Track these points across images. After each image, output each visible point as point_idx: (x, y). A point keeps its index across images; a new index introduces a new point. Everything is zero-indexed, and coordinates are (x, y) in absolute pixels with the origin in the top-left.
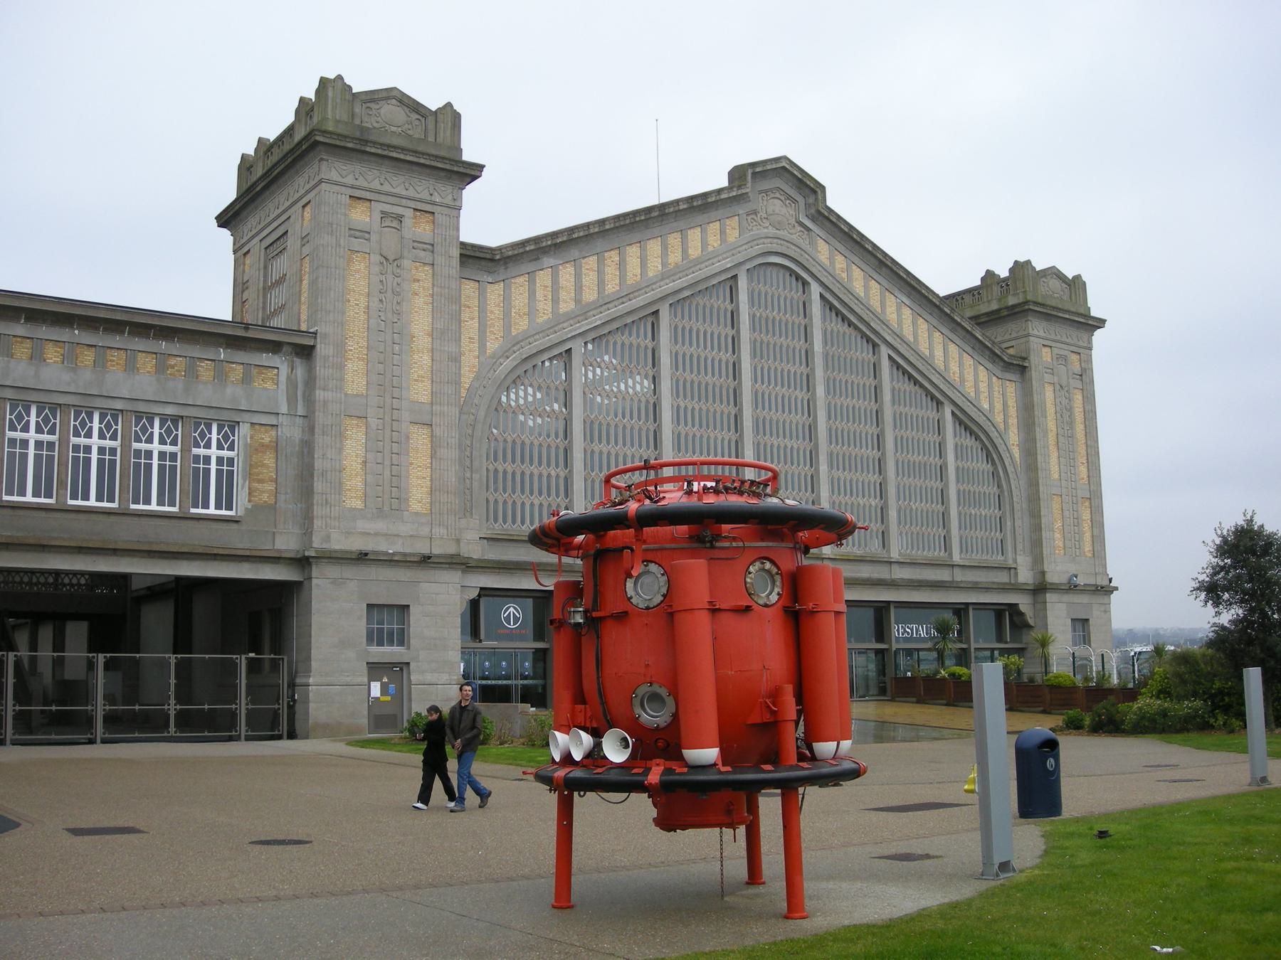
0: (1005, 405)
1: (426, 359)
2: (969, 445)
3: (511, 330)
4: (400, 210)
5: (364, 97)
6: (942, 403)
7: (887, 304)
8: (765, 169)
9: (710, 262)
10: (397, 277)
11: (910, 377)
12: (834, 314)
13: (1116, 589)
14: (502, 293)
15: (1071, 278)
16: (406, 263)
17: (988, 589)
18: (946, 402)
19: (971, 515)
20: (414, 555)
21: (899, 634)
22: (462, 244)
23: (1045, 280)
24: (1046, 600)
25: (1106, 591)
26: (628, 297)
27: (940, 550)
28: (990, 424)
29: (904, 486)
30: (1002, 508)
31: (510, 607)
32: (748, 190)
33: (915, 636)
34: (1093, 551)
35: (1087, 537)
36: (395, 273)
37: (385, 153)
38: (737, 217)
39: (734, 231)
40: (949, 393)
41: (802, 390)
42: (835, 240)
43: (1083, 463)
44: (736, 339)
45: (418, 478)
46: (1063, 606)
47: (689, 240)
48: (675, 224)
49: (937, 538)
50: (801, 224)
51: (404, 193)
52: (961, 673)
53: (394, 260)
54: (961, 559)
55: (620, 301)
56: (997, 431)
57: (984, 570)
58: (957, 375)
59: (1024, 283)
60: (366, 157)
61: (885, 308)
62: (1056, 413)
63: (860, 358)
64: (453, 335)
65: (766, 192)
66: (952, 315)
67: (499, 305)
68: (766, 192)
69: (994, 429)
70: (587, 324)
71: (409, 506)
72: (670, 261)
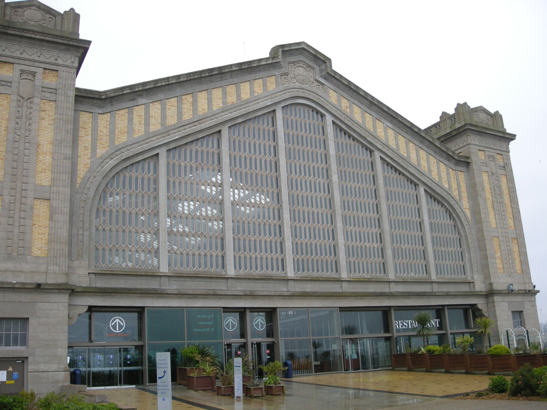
0: (459, 185)
1: (48, 159)
2: (438, 209)
3: (114, 142)
4: (33, 69)
5: (13, 5)
6: (418, 185)
7: (377, 127)
8: (291, 48)
9: (256, 102)
10: (30, 109)
11: (396, 170)
12: (343, 134)
13: (538, 291)
14: (109, 120)
15: (493, 113)
16: (36, 100)
17: (455, 295)
18: (420, 184)
19: (442, 251)
20: (30, 284)
21: (399, 327)
22: (78, 90)
23: (477, 114)
24: (494, 300)
25: (533, 293)
26: (198, 122)
27: (423, 273)
28: (450, 196)
29: (396, 235)
30: (462, 246)
31: (117, 318)
32: (279, 60)
33: (410, 327)
34: (522, 270)
35: (517, 261)
36: (29, 106)
37: (22, 34)
38: (274, 77)
39: (272, 85)
40: (422, 179)
41: (323, 177)
42: (340, 90)
43: (510, 218)
44: (276, 148)
45: (39, 234)
46: (506, 304)
47: (241, 89)
48: (231, 80)
49: (420, 266)
50: (318, 81)
51: (37, 59)
52: (434, 350)
53: (29, 99)
54: (437, 278)
55: (193, 124)
56: (455, 200)
57: (453, 284)
58: (426, 168)
59: (464, 115)
60: (9, 38)
61: (376, 130)
62: (491, 189)
63: (362, 159)
64: (68, 143)
65: (294, 63)
66: (419, 132)
67: (106, 127)
68: (294, 63)
69: (452, 199)
70: (169, 138)
71: (31, 252)
72: (228, 101)
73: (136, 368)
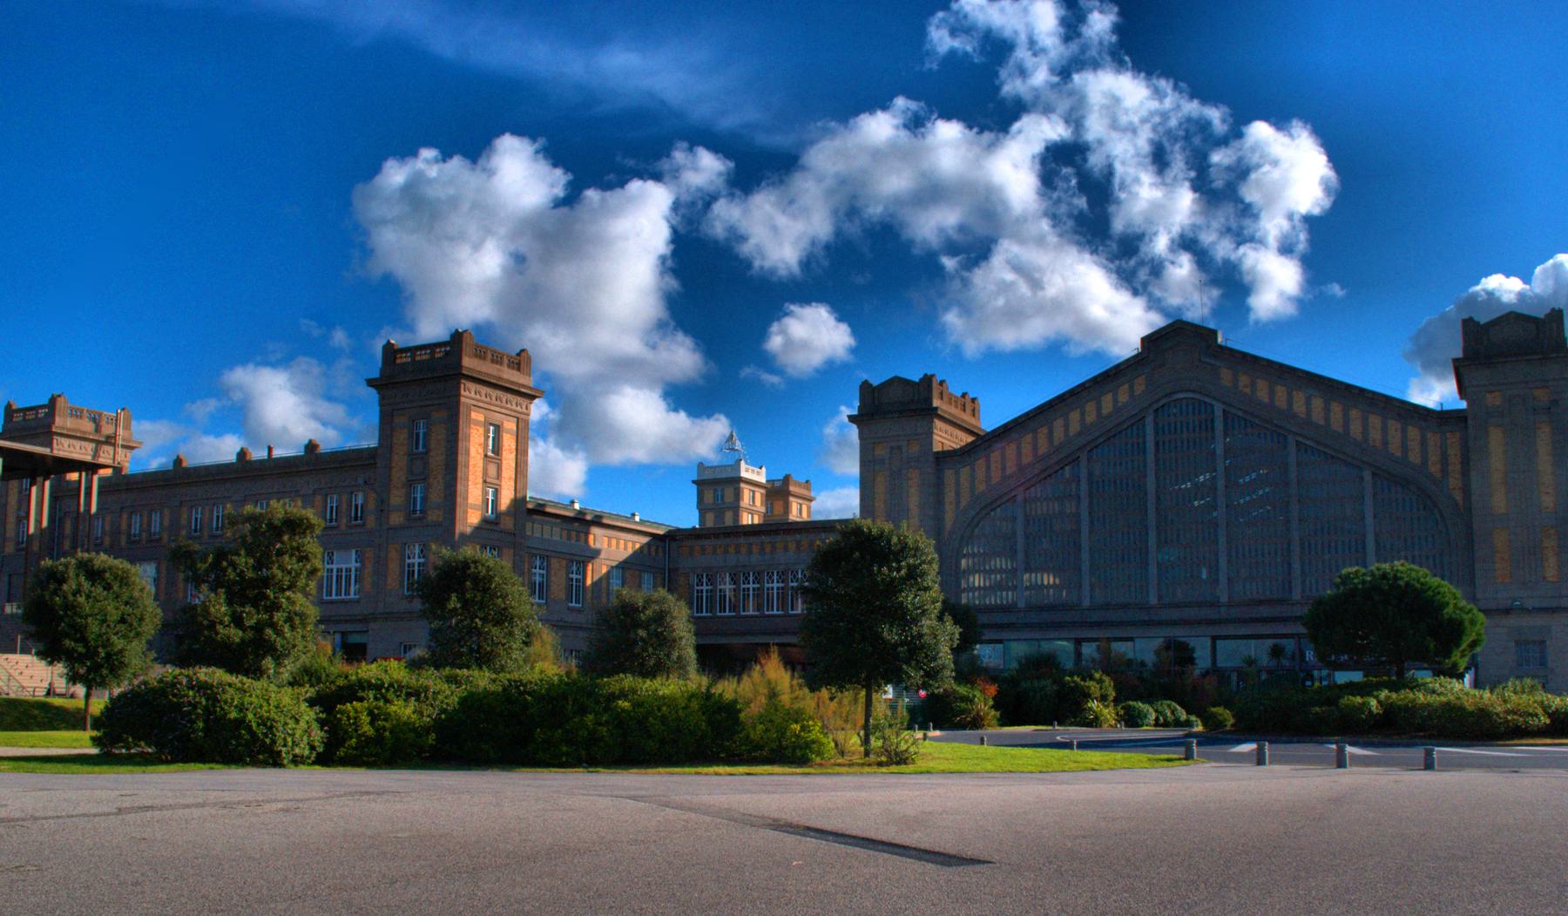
73: (471, 500)
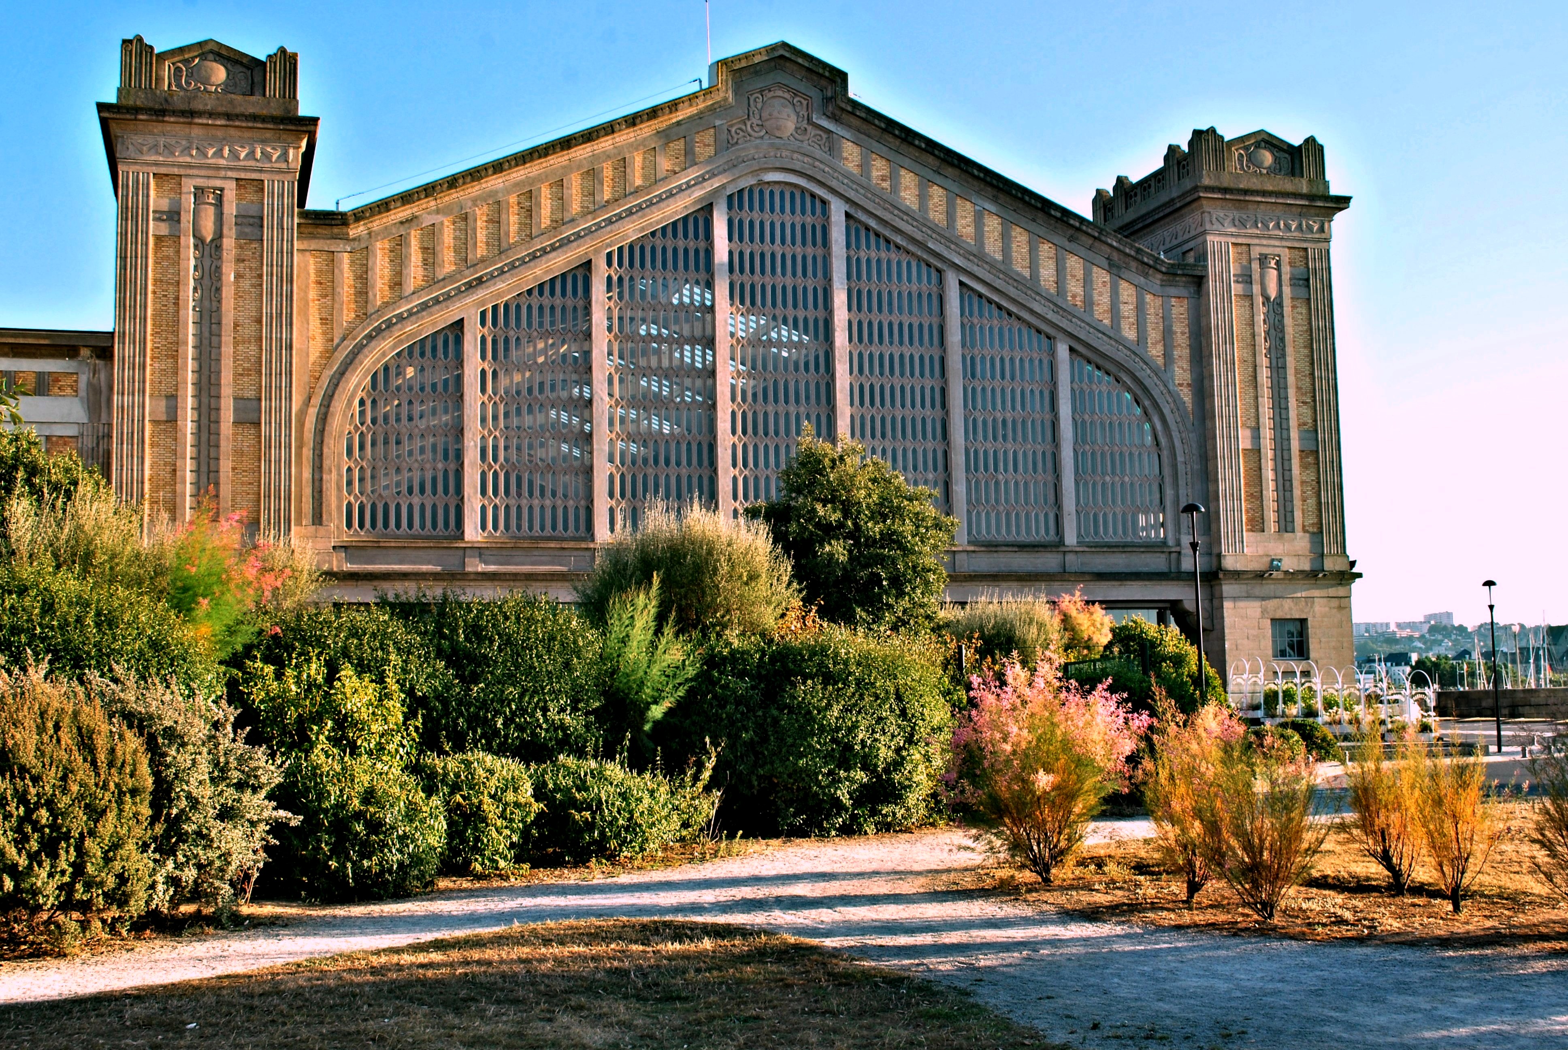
13: (1359, 575)
18: (1060, 336)
38: (712, 131)
